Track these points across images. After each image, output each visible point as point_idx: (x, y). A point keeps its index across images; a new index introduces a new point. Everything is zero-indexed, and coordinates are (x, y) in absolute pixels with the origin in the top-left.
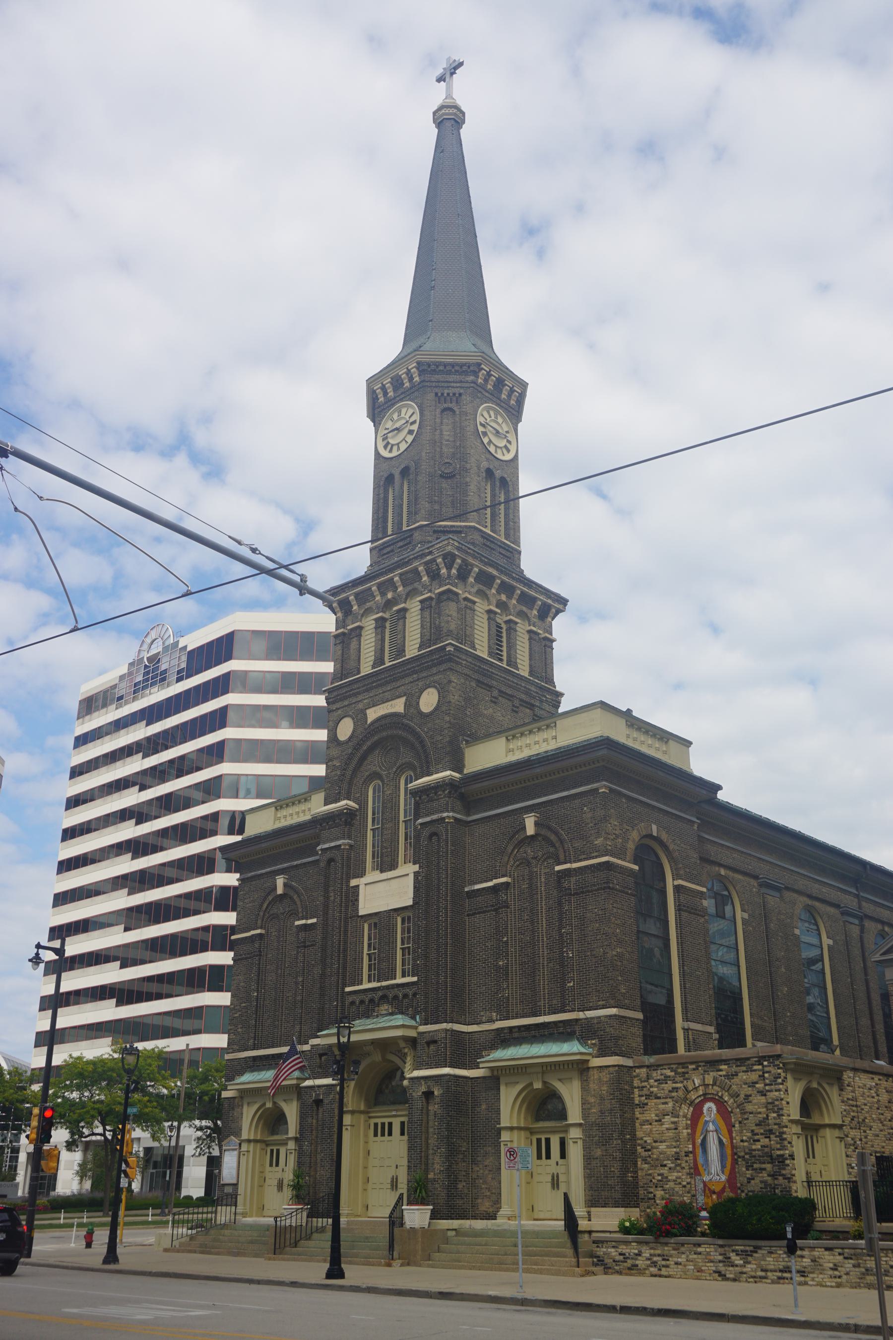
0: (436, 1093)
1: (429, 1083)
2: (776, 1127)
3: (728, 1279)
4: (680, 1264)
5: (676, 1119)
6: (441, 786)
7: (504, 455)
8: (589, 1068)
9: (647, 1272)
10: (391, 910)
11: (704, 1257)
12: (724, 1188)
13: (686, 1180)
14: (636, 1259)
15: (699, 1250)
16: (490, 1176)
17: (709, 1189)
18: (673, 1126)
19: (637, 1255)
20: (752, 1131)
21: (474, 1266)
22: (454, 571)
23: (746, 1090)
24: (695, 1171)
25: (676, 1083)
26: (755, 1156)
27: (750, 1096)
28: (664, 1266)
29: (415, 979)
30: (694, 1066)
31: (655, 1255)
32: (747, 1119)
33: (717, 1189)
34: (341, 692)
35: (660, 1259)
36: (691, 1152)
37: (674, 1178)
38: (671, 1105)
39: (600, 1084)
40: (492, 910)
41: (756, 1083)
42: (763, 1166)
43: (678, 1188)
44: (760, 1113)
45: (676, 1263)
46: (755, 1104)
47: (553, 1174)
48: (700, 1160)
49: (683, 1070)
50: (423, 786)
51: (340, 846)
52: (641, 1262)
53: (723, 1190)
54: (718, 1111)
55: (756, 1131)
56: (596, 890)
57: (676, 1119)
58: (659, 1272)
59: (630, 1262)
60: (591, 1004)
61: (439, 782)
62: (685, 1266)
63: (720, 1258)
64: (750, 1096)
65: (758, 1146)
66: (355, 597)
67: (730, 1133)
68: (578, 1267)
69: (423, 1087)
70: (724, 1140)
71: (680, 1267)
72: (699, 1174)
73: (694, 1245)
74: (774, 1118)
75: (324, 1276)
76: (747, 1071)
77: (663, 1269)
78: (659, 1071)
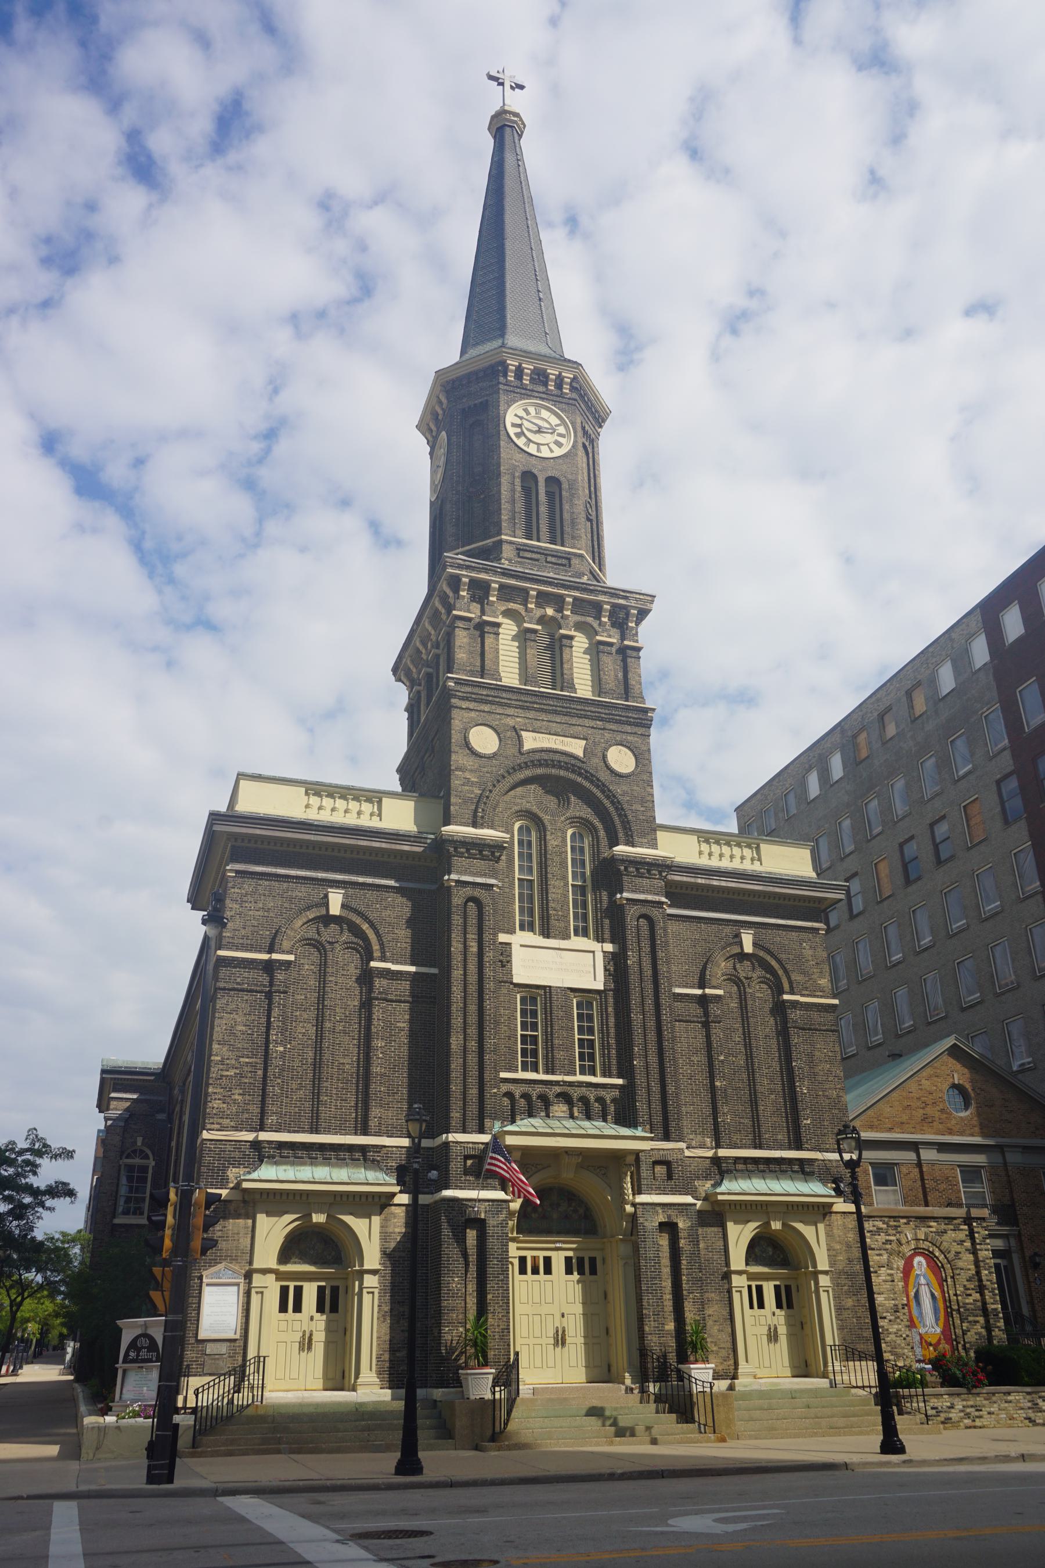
0: (681, 1225)
1: (670, 1212)
2: (989, 1283)
3: (1038, 1424)
4: (993, 1413)
5: (892, 1272)
6: (659, 865)
7: (552, 451)
8: (831, 1213)
9: (961, 1424)
10: (568, 988)
11: (1014, 1405)
12: (940, 1340)
13: (905, 1332)
14: (950, 1412)
15: (1010, 1398)
16: (716, 1327)
17: (926, 1341)
18: (889, 1278)
19: (949, 1408)
20: (965, 1286)
21: (816, 1433)
22: (605, 619)
23: (955, 1248)
24: (912, 1325)
25: (889, 1235)
26: (968, 1310)
27: (960, 1253)
28: (977, 1417)
29: (620, 1081)
30: (905, 1221)
31: (968, 1407)
32: (959, 1274)
33: (934, 1342)
34: (476, 690)
35: (973, 1410)
36: (906, 1305)
37: (895, 1330)
38: (885, 1257)
39: (398, 1220)
40: (698, 1022)
41: (964, 1241)
42: (977, 1319)
43: (899, 1341)
44: (969, 1269)
45: (989, 1413)
46: (965, 1261)
47: (304, 1331)
48: (915, 1313)
49: (895, 1223)
50: (635, 857)
51: (492, 886)
52: (954, 1415)
53: (939, 1342)
54: (928, 1266)
55: (968, 1286)
56: (824, 1031)
57: (892, 1272)
58: (973, 1424)
59: (943, 1415)
60: (828, 1146)
61: (658, 860)
62: (998, 1415)
63: (1029, 1404)
64: (960, 1253)
65: (970, 1300)
66: (638, 613)
67: (941, 1286)
68: (714, 1432)
69: (661, 1216)
70: (936, 1294)
71: (993, 1416)
72: (915, 1327)
73: (1005, 1393)
74: (986, 1275)
75: (393, 1471)
76: (954, 1230)
77: (977, 1420)
78: (871, 1222)
